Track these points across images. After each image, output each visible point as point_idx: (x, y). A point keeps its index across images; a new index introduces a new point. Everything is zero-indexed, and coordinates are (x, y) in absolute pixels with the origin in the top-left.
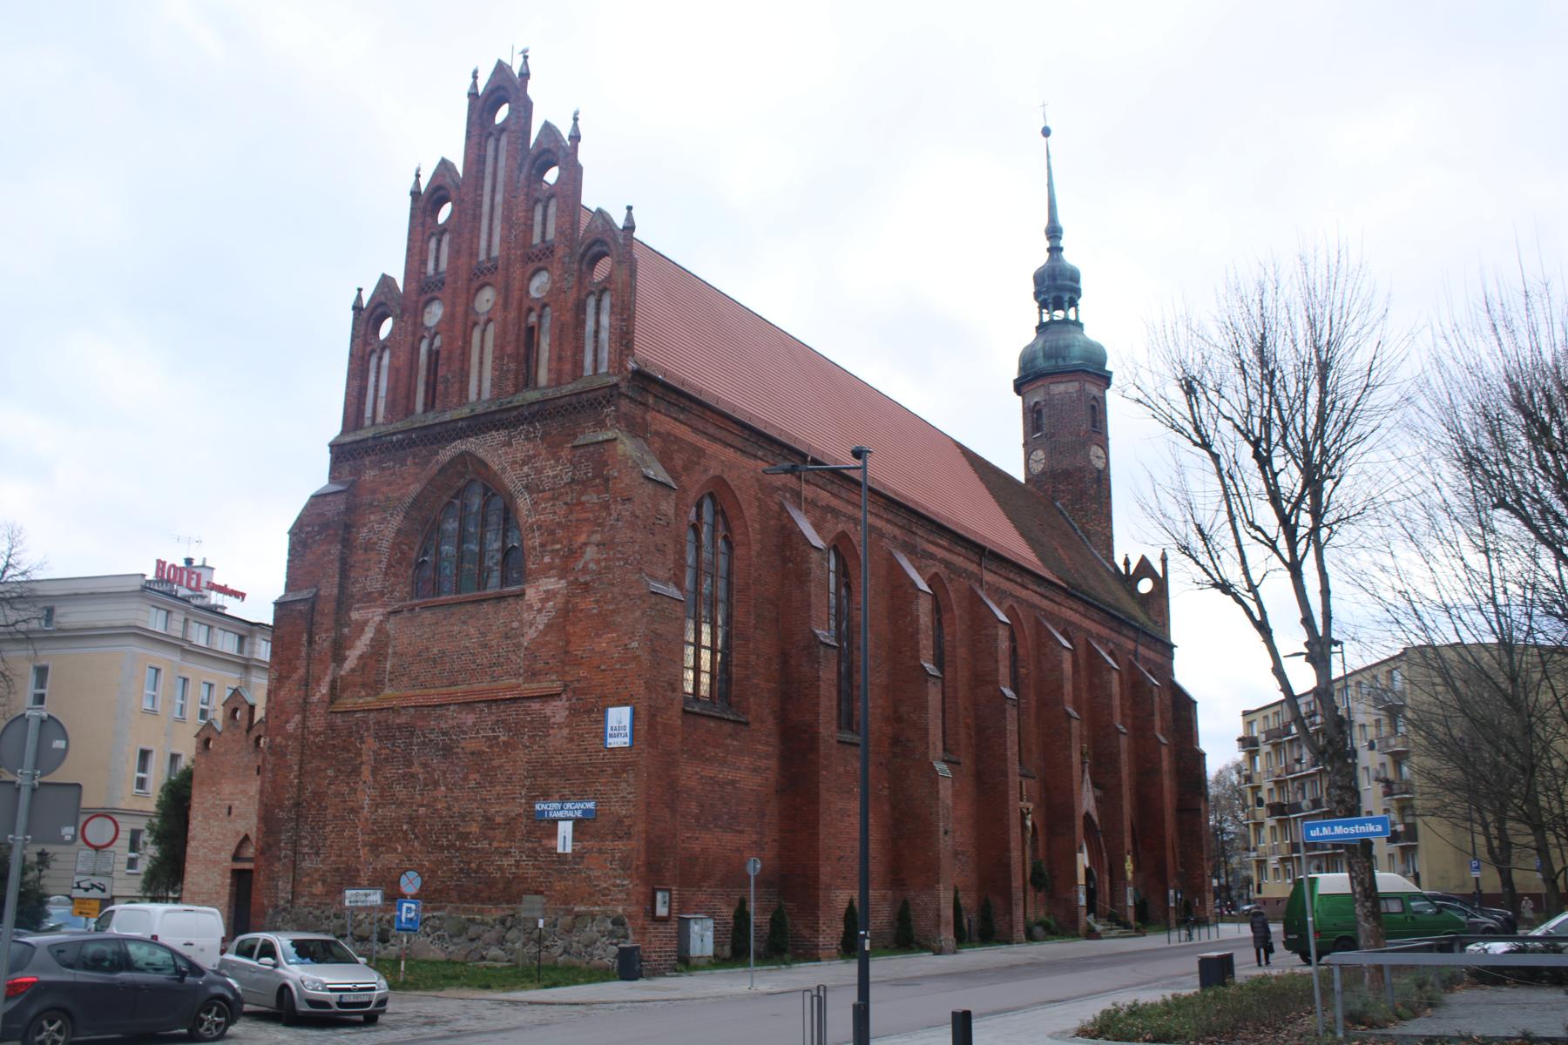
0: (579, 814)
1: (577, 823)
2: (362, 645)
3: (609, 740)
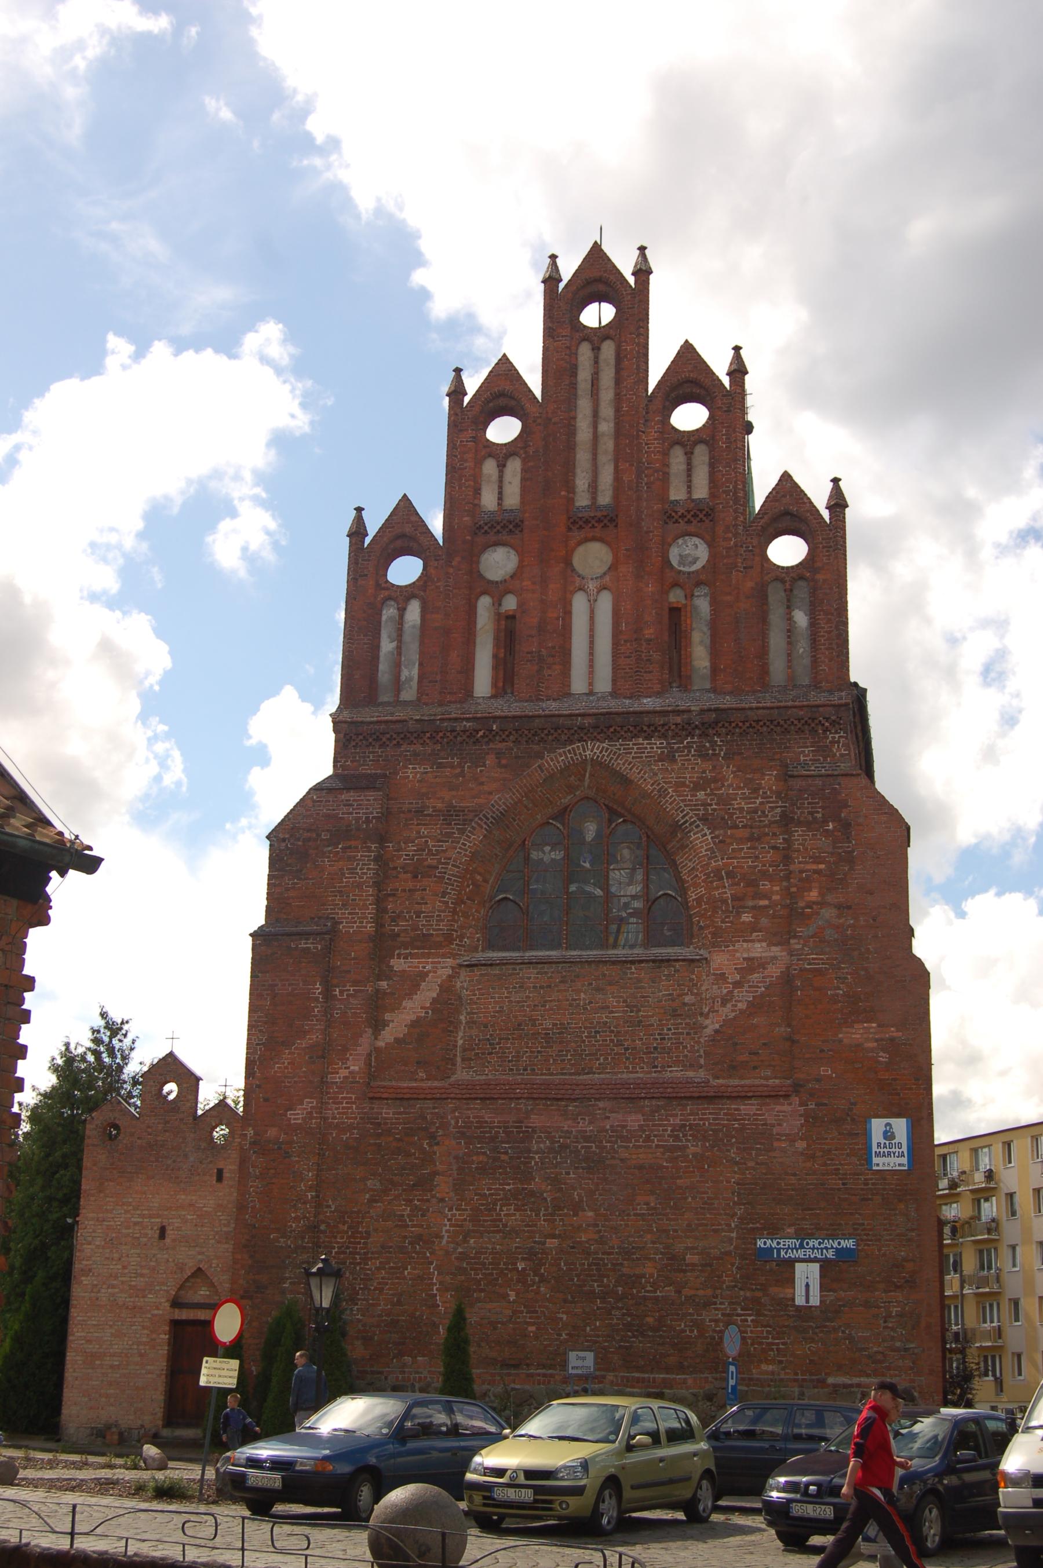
0: (830, 1254)
1: (826, 1266)
2: (415, 1007)
3: (875, 1160)
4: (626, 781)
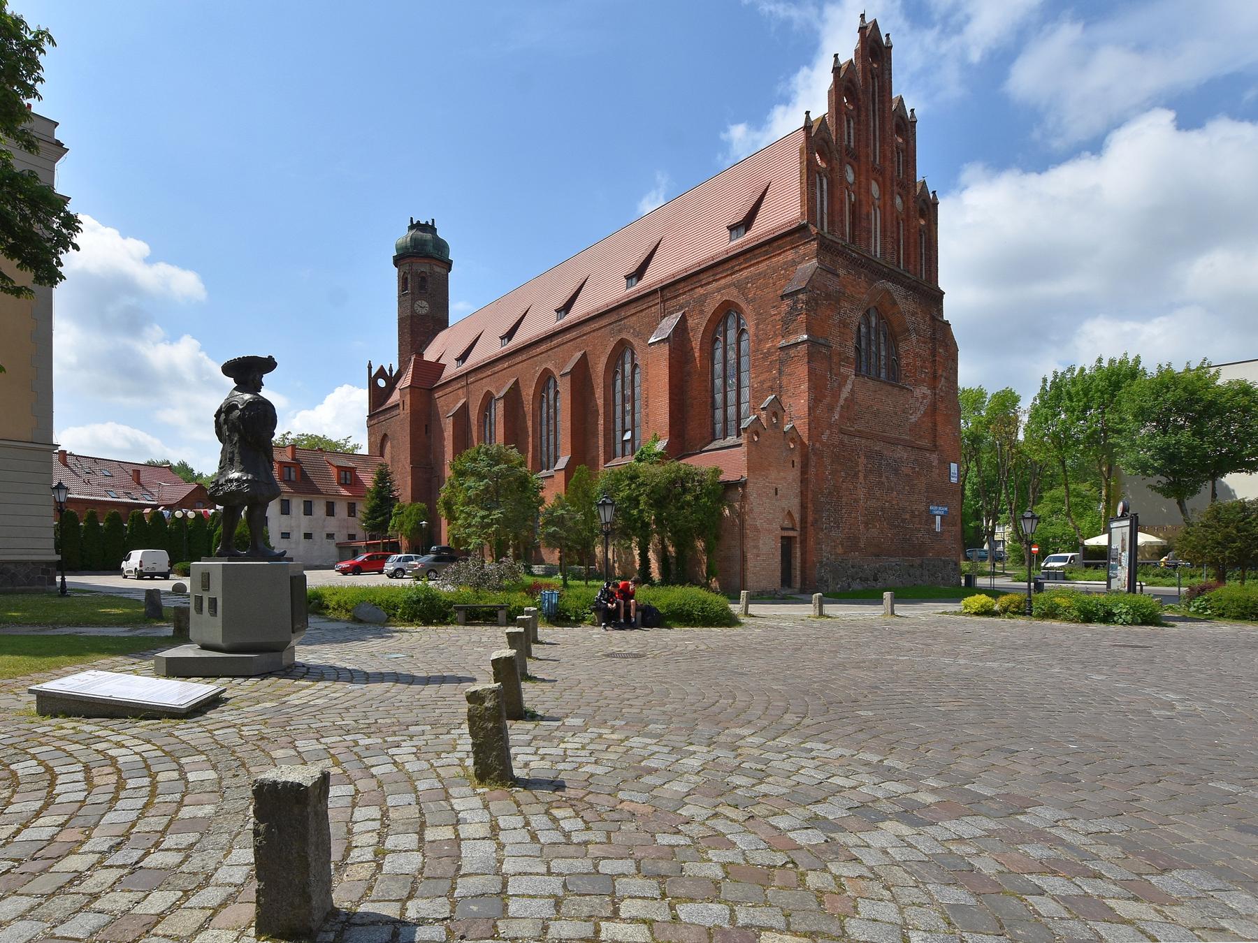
4: (895, 303)
